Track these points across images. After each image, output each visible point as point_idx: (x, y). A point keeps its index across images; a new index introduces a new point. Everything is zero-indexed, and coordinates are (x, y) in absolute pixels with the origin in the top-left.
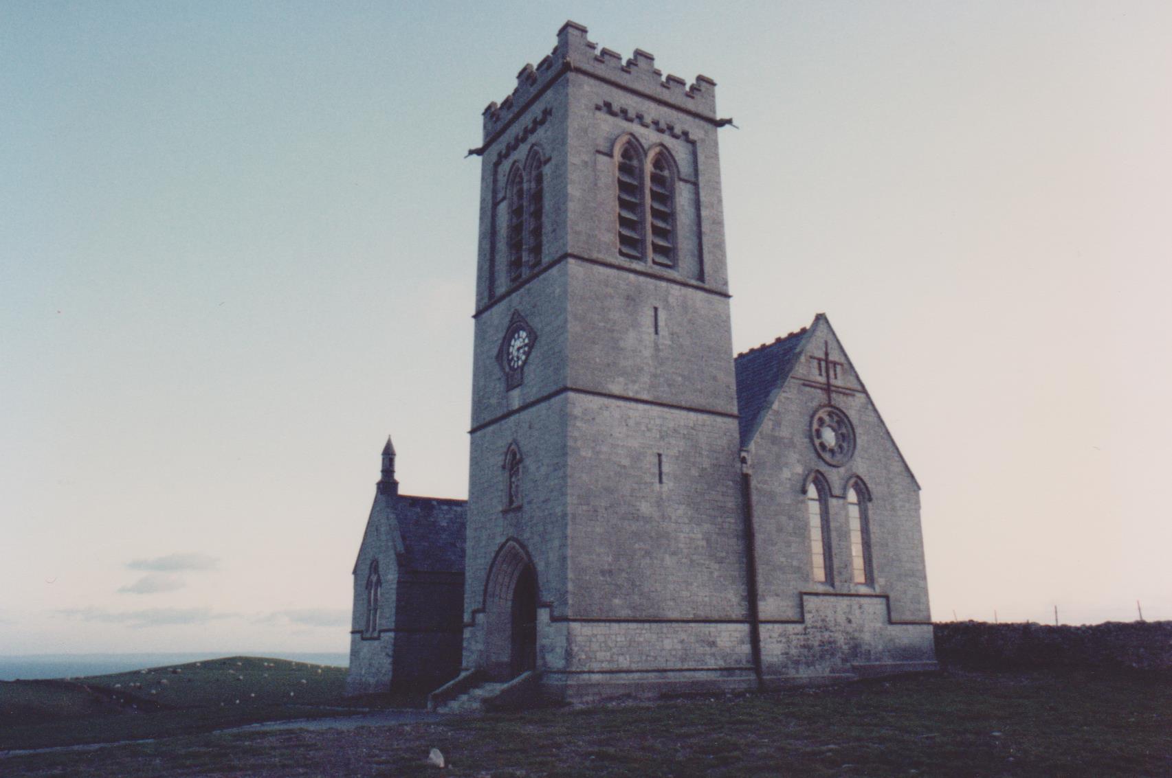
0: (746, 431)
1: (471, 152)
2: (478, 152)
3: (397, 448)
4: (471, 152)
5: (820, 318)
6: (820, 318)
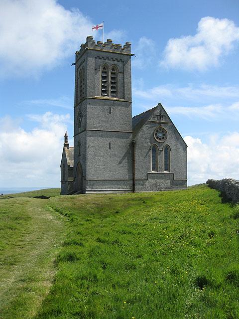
0: (134, 137)
1: (73, 64)
2: (75, 64)
3: (68, 135)
4: (73, 64)
5: (160, 104)
6: (160, 104)
